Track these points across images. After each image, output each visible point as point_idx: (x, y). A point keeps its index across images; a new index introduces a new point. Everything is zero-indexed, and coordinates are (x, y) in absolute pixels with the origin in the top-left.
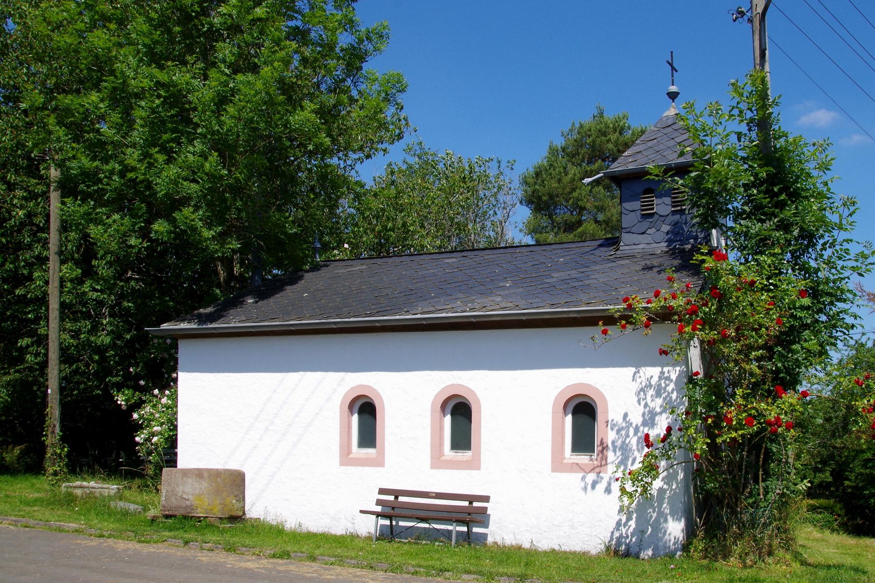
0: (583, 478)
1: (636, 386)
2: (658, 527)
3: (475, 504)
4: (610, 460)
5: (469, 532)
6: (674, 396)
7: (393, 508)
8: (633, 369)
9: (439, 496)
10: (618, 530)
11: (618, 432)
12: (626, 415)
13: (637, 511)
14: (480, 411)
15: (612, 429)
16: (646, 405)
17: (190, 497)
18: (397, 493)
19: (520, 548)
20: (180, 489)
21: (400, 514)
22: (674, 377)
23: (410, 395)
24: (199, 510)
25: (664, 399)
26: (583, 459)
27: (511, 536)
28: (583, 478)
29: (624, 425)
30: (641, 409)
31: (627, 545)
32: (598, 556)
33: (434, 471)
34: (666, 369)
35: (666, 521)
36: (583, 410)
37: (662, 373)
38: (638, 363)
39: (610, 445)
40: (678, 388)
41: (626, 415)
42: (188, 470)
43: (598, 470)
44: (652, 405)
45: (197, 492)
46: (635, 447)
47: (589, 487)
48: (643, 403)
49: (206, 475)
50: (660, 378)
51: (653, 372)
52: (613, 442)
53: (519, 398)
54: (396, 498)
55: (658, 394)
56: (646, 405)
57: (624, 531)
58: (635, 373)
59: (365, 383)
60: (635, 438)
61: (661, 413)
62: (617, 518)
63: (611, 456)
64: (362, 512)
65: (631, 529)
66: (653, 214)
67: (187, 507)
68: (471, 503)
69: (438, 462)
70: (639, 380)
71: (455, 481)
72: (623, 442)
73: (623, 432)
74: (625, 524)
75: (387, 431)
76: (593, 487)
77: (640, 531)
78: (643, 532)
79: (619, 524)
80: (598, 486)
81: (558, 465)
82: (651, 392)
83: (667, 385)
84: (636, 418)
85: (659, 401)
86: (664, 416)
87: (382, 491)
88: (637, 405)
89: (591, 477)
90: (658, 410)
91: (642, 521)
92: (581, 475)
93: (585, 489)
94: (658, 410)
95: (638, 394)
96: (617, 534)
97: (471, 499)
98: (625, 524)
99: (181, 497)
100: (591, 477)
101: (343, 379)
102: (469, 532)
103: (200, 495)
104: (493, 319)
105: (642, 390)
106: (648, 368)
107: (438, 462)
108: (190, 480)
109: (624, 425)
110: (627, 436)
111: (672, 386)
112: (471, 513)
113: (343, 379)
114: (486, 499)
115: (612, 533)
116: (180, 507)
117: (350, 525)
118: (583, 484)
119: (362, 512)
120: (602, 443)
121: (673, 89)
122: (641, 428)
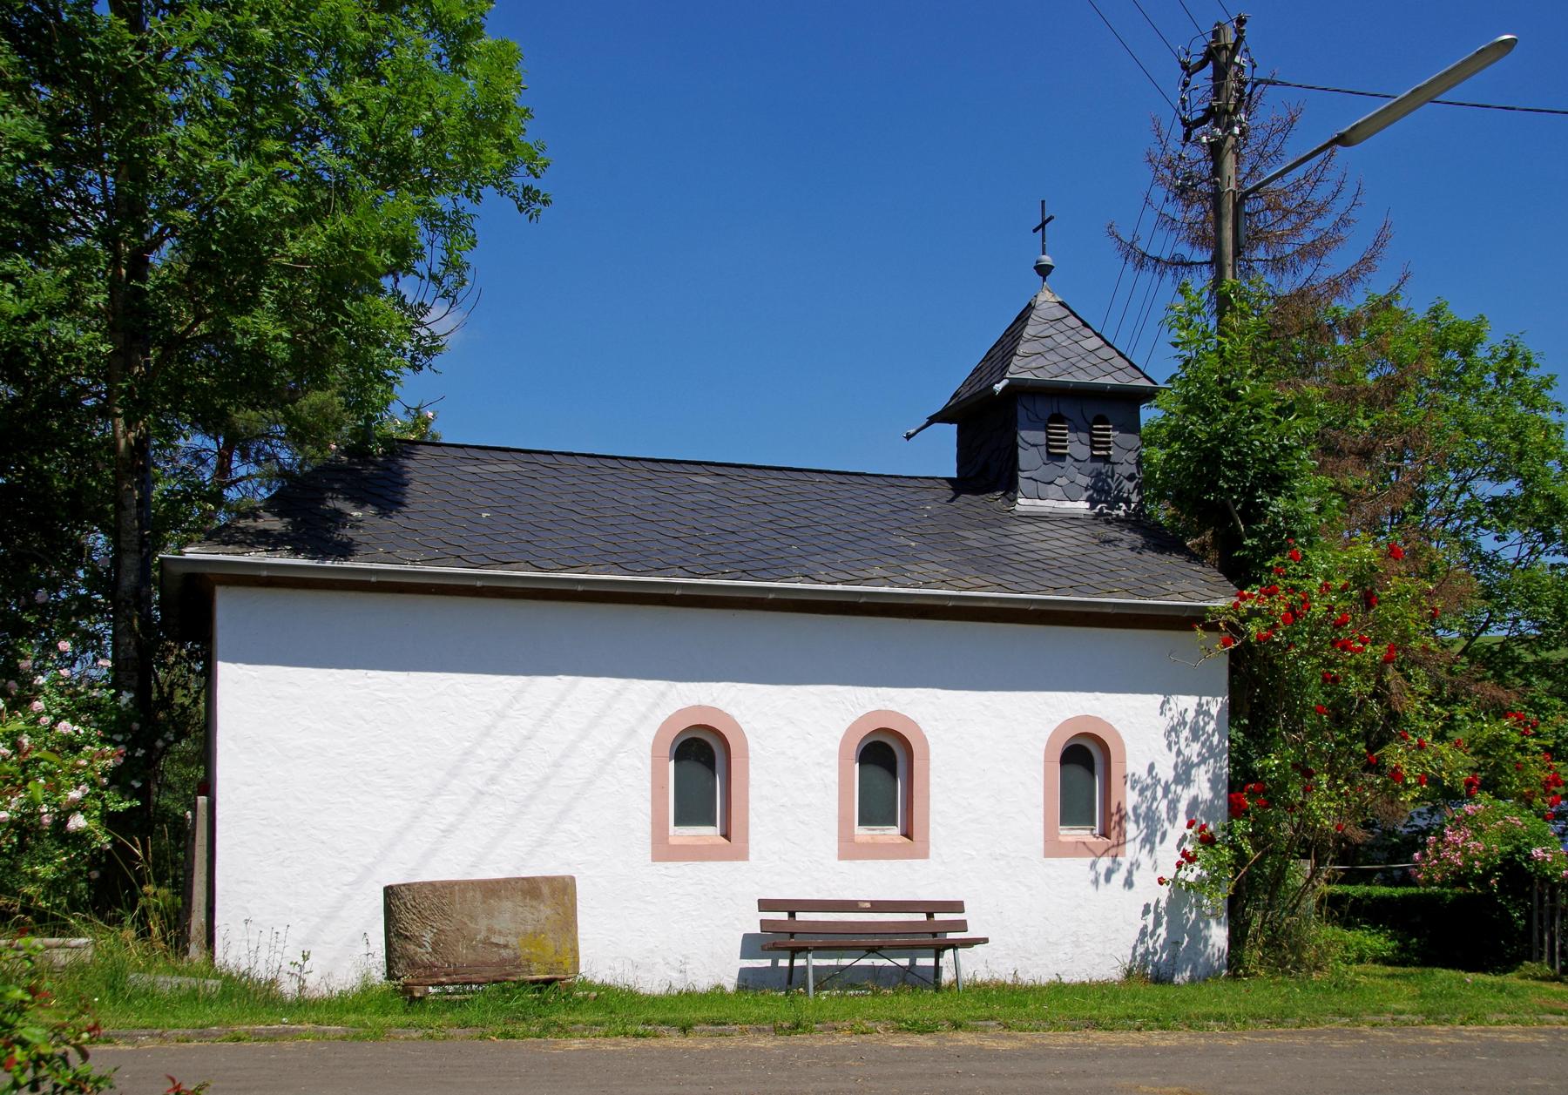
0: (1093, 865)
1: (1164, 723)
2: (1198, 937)
3: (938, 917)
4: (1129, 836)
5: (913, 964)
6: (1215, 739)
7: (792, 935)
8: (1161, 698)
9: (877, 906)
10: (1142, 942)
11: (1142, 792)
12: (1152, 767)
13: (1168, 910)
14: (927, 759)
15: (1133, 788)
16: (1179, 753)
17: (512, 941)
18: (792, 907)
19: (1083, 983)
20: (483, 924)
21: (797, 950)
22: (1214, 710)
23: (793, 731)
24: (535, 966)
25: (1203, 744)
26: (1081, 834)
27: (981, 967)
28: (1093, 865)
29: (1149, 781)
30: (1171, 758)
31: (1155, 965)
32: (1121, 983)
33: (845, 863)
34: (1204, 699)
35: (1207, 925)
36: (1083, 759)
37: (1200, 705)
38: (1168, 687)
39: (1130, 813)
40: (1218, 729)
41: (1152, 767)
42: (497, 881)
43: (1113, 851)
44: (1187, 752)
45: (530, 929)
46: (1164, 816)
47: (1102, 879)
48: (1175, 749)
49: (546, 890)
50: (1198, 713)
51: (1188, 703)
52: (1135, 809)
53: (987, 740)
54: (930, 915)
55: (1195, 738)
56: (1179, 753)
57: (1151, 944)
58: (1163, 703)
59: (706, 702)
60: (1165, 802)
61: (1198, 765)
62: (1141, 924)
63: (1131, 829)
64: (985, 941)
65: (1161, 941)
66: (1064, 455)
67: (503, 962)
68: (930, 915)
69: (849, 850)
70: (1169, 714)
71: (883, 879)
72: (1149, 808)
73: (1148, 793)
74: (1153, 933)
75: (753, 793)
76: (1108, 879)
77: (1173, 943)
78: (1177, 943)
79: (1143, 932)
80: (1114, 877)
81: (1054, 849)
82: (1186, 733)
83: (1206, 724)
84: (1166, 772)
85: (1196, 747)
86: (1203, 768)
87: (765, 905)
88: (1166, 750)
89: (1104, 863)
90: (1195, 759)
91: (1176, 927)
92: (1089, 860)
93: (1096, 882)
94: (1195, 759)
95: (1168, 734)
96: (1140, 950)
97: (930, 908)
98: (1153, 933)
99: (487, 943)
100: (1104, 863)
101: (619, 693)
102: (913, 964)
103: (535, 934)
104: (985, 604)
105: (1173, 729)
106: (1181, 697)
107: (849, 850)
108: (508, 905)
109: (1149, 781)
110: (1154, 799)
111: (1211, 727)
112: (934, 930)
113: (663, 695)
114: (957, 907)
115: (1135, 948)
116: (485, 964)
117: (675, 975)
118: (1092, 875)
119: (985, 941)
120: (1119, 810)
121: (1047, 260)
122: (1173, 787)
